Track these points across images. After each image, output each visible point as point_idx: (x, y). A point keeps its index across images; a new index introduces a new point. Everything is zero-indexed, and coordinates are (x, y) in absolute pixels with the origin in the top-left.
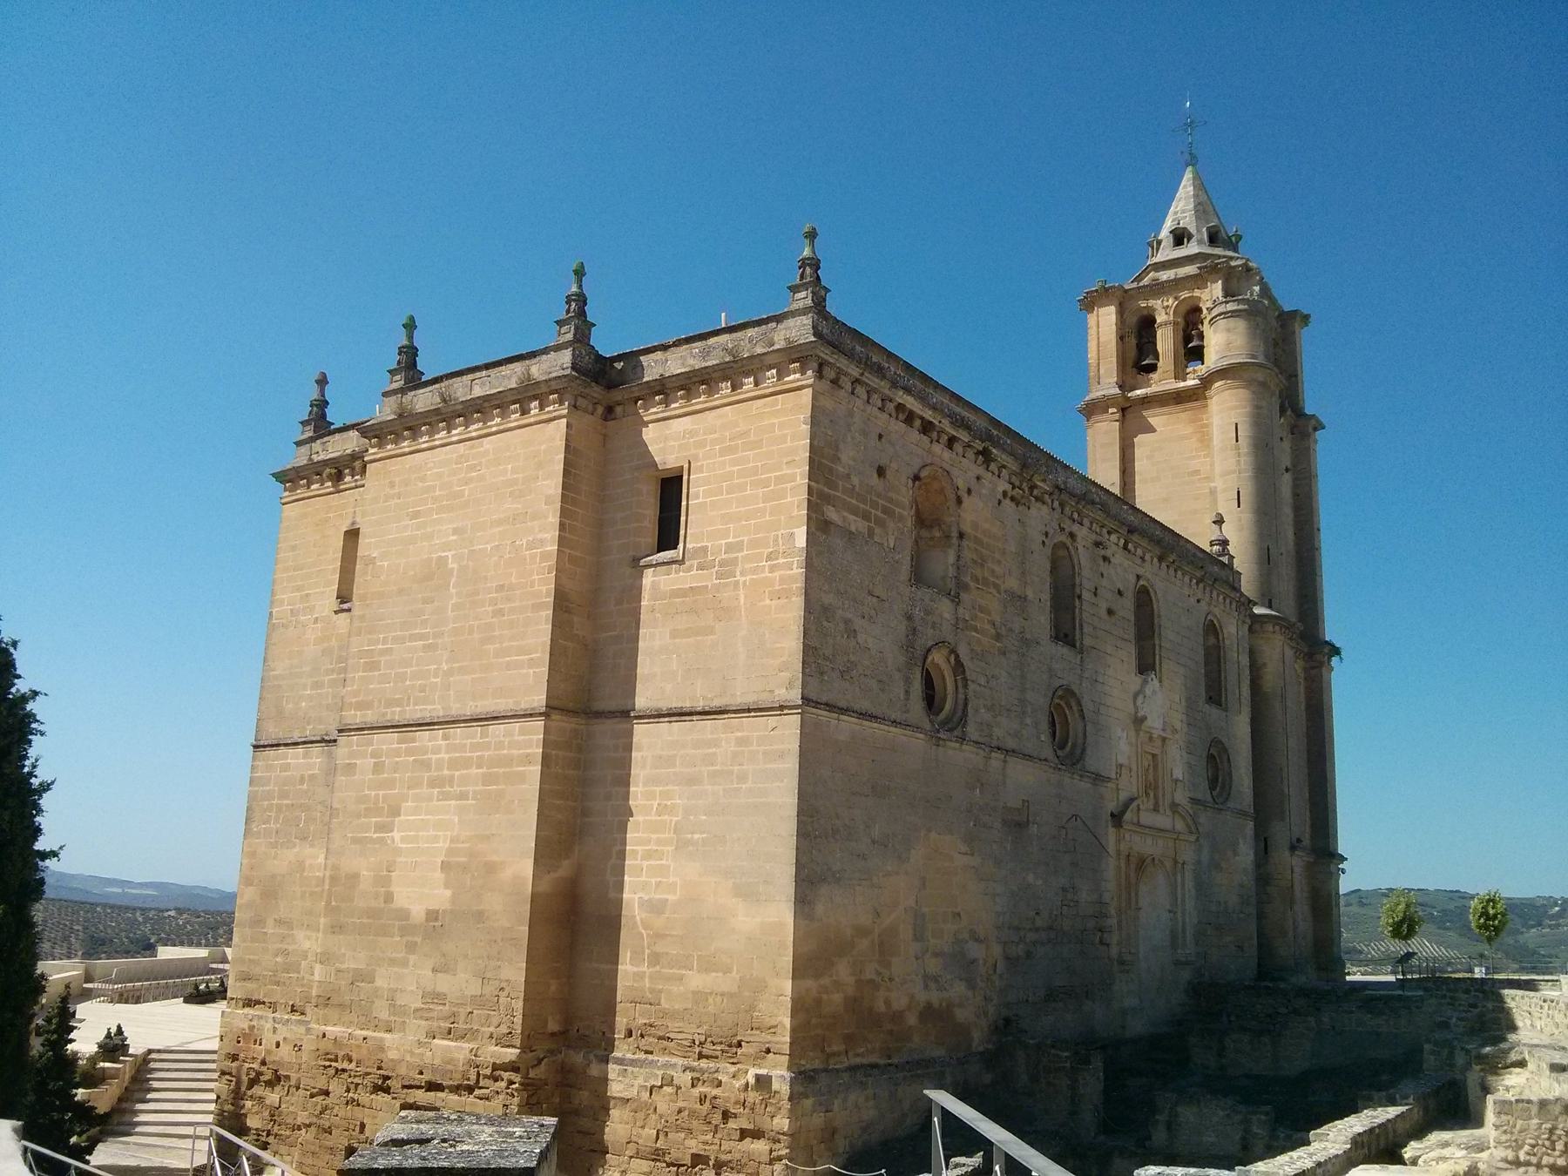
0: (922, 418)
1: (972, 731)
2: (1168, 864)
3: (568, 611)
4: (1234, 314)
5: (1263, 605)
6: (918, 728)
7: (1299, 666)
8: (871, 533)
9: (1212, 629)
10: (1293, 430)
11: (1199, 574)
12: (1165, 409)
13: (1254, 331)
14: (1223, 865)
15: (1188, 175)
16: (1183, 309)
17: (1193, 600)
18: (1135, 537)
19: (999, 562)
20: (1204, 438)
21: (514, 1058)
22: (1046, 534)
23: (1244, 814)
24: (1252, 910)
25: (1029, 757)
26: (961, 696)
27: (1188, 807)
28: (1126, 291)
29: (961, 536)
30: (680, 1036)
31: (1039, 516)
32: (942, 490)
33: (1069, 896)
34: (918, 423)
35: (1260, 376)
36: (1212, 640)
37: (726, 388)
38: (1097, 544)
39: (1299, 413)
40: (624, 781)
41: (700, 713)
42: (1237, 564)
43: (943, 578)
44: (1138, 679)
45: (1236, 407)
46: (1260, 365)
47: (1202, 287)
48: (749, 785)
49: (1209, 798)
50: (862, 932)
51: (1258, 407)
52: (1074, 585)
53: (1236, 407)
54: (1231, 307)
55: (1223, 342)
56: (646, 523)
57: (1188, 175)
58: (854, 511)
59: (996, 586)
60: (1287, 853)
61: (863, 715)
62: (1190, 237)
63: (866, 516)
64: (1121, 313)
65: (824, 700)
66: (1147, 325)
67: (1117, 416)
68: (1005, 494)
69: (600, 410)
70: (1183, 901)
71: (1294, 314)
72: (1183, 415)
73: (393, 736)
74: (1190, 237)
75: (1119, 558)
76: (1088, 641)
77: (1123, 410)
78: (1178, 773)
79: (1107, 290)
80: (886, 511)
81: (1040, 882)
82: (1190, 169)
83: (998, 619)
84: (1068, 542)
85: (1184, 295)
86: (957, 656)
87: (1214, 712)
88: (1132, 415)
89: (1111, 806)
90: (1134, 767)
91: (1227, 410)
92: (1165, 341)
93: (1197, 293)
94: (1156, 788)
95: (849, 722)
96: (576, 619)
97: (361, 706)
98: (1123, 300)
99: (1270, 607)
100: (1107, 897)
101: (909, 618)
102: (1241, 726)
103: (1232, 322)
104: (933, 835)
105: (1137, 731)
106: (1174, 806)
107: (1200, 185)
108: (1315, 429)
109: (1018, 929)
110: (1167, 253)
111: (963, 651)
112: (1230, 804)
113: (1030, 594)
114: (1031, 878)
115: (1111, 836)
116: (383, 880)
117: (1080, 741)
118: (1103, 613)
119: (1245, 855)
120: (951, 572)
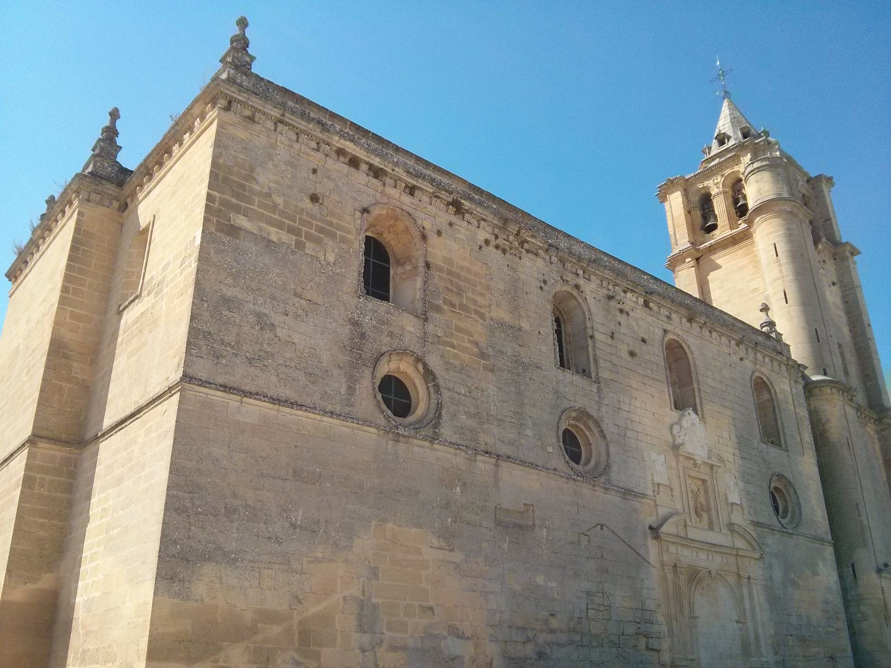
0: (367, 163)
1: (447, 431)
2: (732, 580)
3: (65, 356)
4: (759, 169)
5: (818, 374)
6: (366, 422)
7: (871, 429)
8: (300, 245)
9: (761, 386)
10: (835, 256)
11: (738, 337)
12: (726, 251)
13: (777, 178)
15: (726, 103)
16: (730, 182)
17: (735, 358)
18: (655, 298)
19: (482, 295)
20: (756, 264)
22: (545, 282)
23: (822, 541)
24: (842, 624)
25: (532, 465)
26: (434, 402)
27: (751, 529)
28: (687, 180)
29: (428, 266)
31: (532, 268)
32: (407, 230)
33: (598, 600)
34: (364, 167)
35: (788, 208)
36: (766, 396)
37: (175, 148)
38: (610, 298)
39: (835, 243)
40: (89, 497)
42: (786, 339)
43: (412, 302)
44: (675, 415)
45: (772, 233)
46: (785, 199)
47: (738, 163)
50: (270, 617)
51: (789, 229)
52: (585, 329)
53: (772, 233)
54: (756, 165)
55: (757, 190)
57: (726, 103)
58: (279, 226)
59: (482, 316)
60: (875, 576)
61: (276, 401)
62: (729, 138)
63: (291, 230)
64: (686, 194)
65: (221, 380)
66: (706, 200)
67: (692, 263)
68: (487, 242)
69: (116, 204)
70: (753, 610)
71: (819, 178)
72: (740, 252)
74: (729, 138)
75: (640, 313)
76: (604, 374)
77: (697, 259)
78: (735, 497)
79: (672, 181)
80: (321, 230)
82: (726, 100)
83: (483, 341)
84: (575, 293)
85: (728, 172)
86: (425, 365)
87: (773, 451)
88: (702, 259)
89: (652, 520)
90: (676, 488)
91: (768, 234)
92: (720, 206)
93: (736, 168)
94: (708, 511)
95: (255, 409)
96: (75, 364)
98: (686, 187)
99: (825, 374)
100: (650, 605)
101: (355, 324)
102: (807, 467)
103: (759, 176)
104: (390, 526)
105: (677, 456)
106: (731, 526)
107: (733, 107)
108: (852, 254)
109: (524, 629)
110: (716, 149)
111: (434, 362)
113: (525, 325)
114: (540, 579)
115: (652, 550)
117: (603, 458)
118: (624, 354)
119: (827, 575)
120: (419, 295)
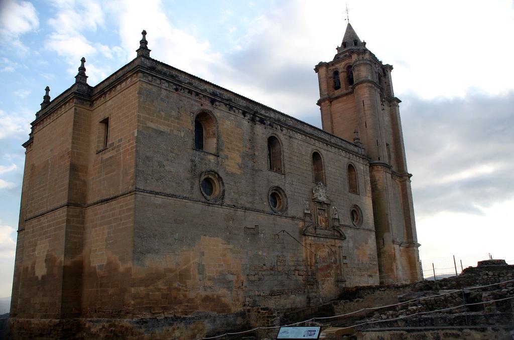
1: (227, 201)
14: (360, 248)
21: (58, 322)
30: (107, 311)
41: (111, 199)
48: (123, 221)
49: (352, 225)
56: (102, 139)
63: (169, 126)
73: (36, 220)
76: (287, 171)
81: (265, 254)
86: (218, 175)
87: (354, 196)
97: (31, 212)
101: (192, 161)
112: (363, 227)
116: (33, 268)
